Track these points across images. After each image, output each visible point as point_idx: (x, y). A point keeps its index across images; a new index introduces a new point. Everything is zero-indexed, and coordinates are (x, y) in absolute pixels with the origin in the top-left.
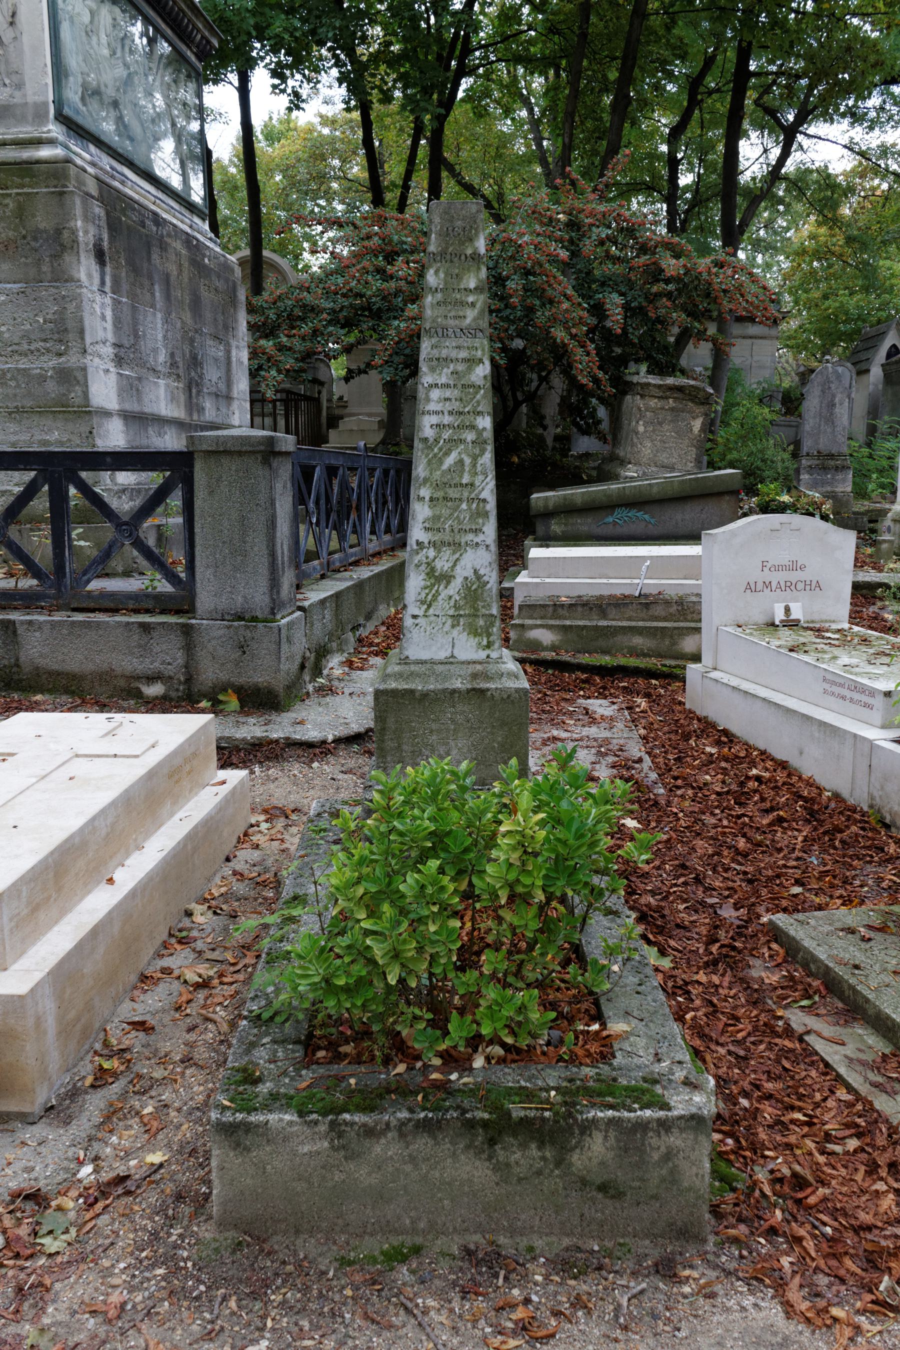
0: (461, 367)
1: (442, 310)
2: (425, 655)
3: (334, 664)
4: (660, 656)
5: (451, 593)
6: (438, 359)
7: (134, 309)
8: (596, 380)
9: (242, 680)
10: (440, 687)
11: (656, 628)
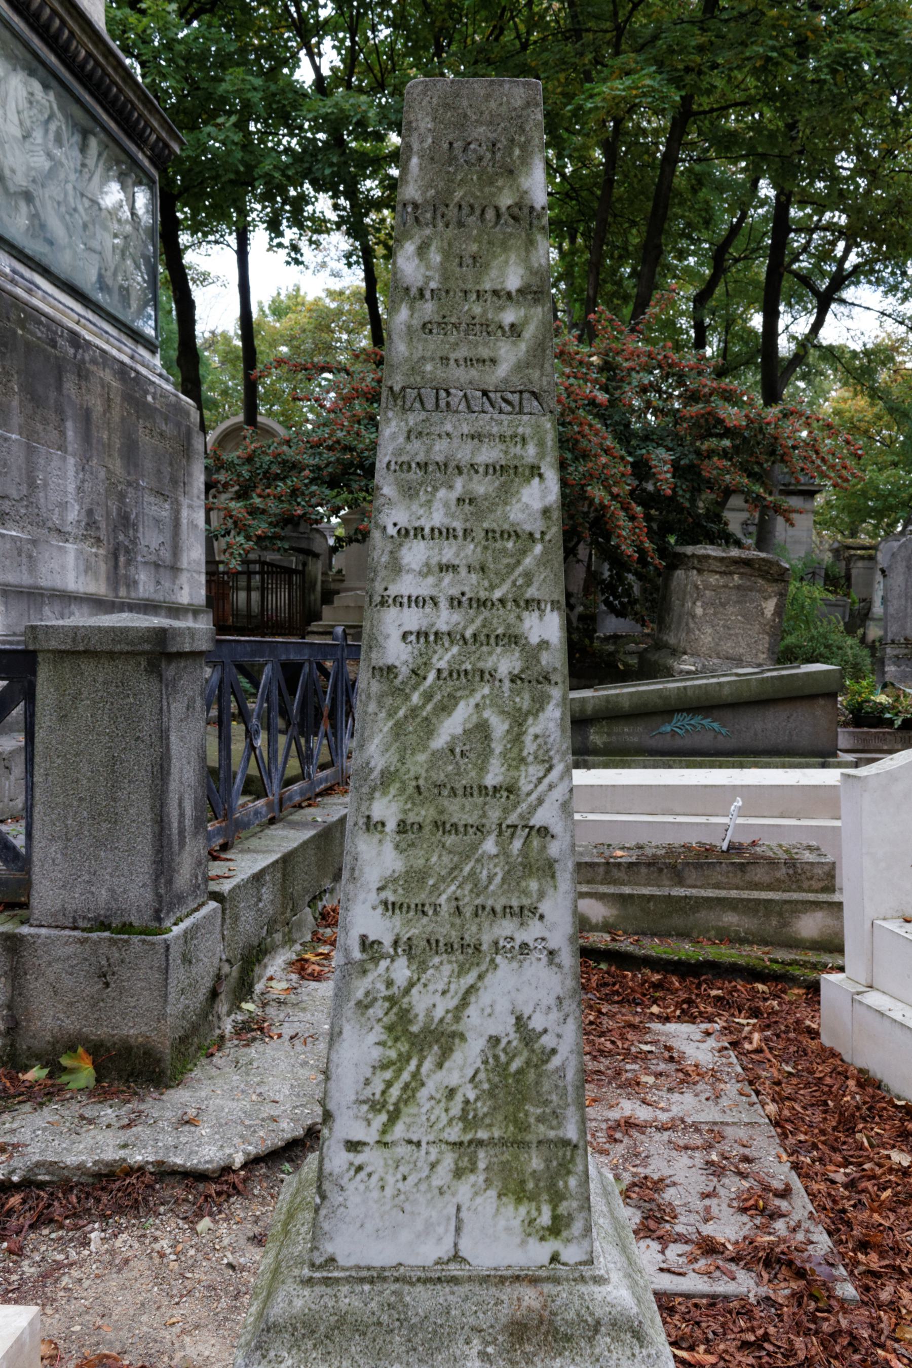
0: (482, 487)
1: (434, 344)
2: (380, 1255)
3: (276, 970)
4: (764, 942)
5: (454, 1079)
6: (423, 466)
7: (30, 450)
8: (641, 551)
9: (103, 1032)
11: (758, 902)
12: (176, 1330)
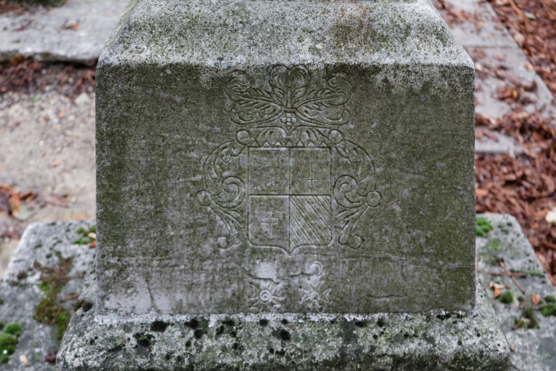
10: (260, 60)
12: (59, 169)
